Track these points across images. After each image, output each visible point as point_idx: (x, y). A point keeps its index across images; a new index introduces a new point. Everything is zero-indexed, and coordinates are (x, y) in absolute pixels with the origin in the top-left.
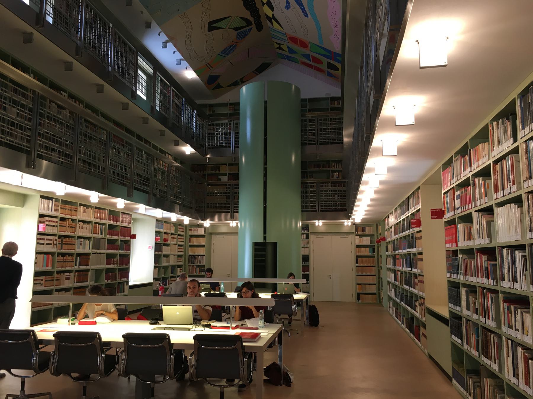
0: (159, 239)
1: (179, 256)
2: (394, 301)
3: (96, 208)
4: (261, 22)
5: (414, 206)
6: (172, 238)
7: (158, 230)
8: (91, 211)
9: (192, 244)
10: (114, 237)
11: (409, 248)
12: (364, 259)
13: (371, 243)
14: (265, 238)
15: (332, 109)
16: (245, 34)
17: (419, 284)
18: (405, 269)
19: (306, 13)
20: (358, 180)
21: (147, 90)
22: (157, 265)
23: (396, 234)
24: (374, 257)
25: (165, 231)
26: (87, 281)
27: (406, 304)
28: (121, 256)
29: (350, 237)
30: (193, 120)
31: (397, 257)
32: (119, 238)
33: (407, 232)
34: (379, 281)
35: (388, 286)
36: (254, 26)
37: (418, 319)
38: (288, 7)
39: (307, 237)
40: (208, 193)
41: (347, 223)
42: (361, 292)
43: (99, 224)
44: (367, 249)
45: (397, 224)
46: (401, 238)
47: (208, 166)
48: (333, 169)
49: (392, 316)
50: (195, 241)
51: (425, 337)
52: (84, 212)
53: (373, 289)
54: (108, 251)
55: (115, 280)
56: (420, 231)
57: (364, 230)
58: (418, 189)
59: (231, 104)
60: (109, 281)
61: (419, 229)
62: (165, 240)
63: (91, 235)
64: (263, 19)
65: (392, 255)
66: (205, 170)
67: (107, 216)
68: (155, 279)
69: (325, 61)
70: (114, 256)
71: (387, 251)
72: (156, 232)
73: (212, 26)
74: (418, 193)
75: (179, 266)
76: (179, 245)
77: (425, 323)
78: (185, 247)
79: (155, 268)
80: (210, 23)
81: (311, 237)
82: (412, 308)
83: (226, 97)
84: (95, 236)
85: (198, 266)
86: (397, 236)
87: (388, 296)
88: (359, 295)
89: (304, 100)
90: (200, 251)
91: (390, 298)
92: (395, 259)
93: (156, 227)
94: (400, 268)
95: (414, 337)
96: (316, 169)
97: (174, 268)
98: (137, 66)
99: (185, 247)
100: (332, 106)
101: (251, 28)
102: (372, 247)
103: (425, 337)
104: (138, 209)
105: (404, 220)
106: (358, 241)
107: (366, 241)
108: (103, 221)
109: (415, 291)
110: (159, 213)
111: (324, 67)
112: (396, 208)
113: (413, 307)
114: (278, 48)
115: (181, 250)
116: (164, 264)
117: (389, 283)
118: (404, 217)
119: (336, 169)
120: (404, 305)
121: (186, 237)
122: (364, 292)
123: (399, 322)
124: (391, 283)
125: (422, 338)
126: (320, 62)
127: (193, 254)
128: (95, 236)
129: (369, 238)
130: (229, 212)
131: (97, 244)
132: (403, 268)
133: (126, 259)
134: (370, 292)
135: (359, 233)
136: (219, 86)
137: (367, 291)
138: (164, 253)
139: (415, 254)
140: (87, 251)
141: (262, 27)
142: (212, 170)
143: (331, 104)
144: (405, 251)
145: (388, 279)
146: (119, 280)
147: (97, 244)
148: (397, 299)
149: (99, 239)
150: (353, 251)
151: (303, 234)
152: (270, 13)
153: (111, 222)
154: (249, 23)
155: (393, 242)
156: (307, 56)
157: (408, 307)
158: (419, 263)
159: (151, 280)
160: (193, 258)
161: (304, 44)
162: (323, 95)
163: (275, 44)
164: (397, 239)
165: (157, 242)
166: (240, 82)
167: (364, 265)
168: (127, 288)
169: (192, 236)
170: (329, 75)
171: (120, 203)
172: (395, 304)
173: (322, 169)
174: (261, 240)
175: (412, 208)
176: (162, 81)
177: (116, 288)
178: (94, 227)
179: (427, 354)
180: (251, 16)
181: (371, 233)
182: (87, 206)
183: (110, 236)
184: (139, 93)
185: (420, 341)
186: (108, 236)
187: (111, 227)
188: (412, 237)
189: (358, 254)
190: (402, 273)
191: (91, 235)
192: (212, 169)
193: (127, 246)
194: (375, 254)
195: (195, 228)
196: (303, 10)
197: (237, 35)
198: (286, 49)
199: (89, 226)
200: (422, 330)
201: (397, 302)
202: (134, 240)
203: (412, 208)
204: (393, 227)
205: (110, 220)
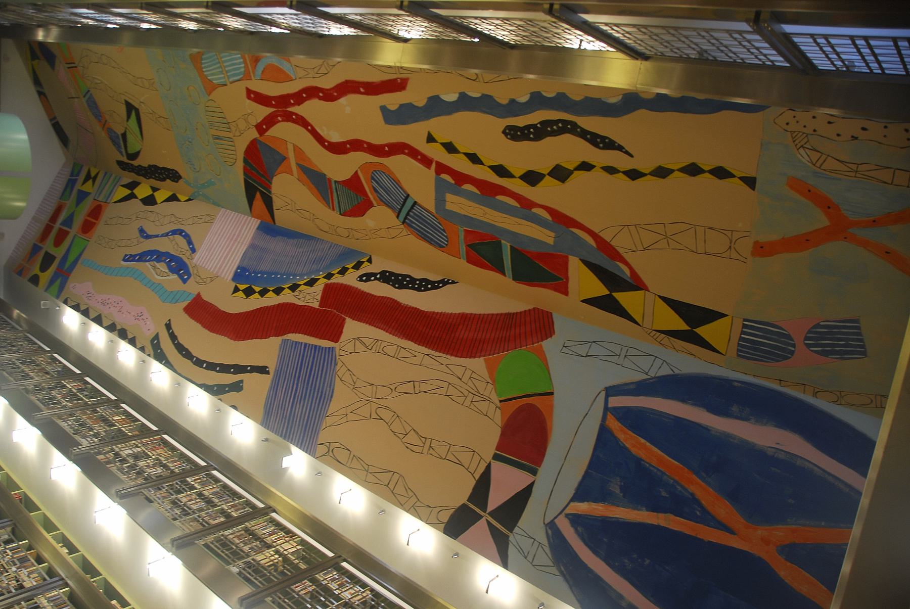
36: (125, 159)
156: (69, 221)
161: (87, 227)
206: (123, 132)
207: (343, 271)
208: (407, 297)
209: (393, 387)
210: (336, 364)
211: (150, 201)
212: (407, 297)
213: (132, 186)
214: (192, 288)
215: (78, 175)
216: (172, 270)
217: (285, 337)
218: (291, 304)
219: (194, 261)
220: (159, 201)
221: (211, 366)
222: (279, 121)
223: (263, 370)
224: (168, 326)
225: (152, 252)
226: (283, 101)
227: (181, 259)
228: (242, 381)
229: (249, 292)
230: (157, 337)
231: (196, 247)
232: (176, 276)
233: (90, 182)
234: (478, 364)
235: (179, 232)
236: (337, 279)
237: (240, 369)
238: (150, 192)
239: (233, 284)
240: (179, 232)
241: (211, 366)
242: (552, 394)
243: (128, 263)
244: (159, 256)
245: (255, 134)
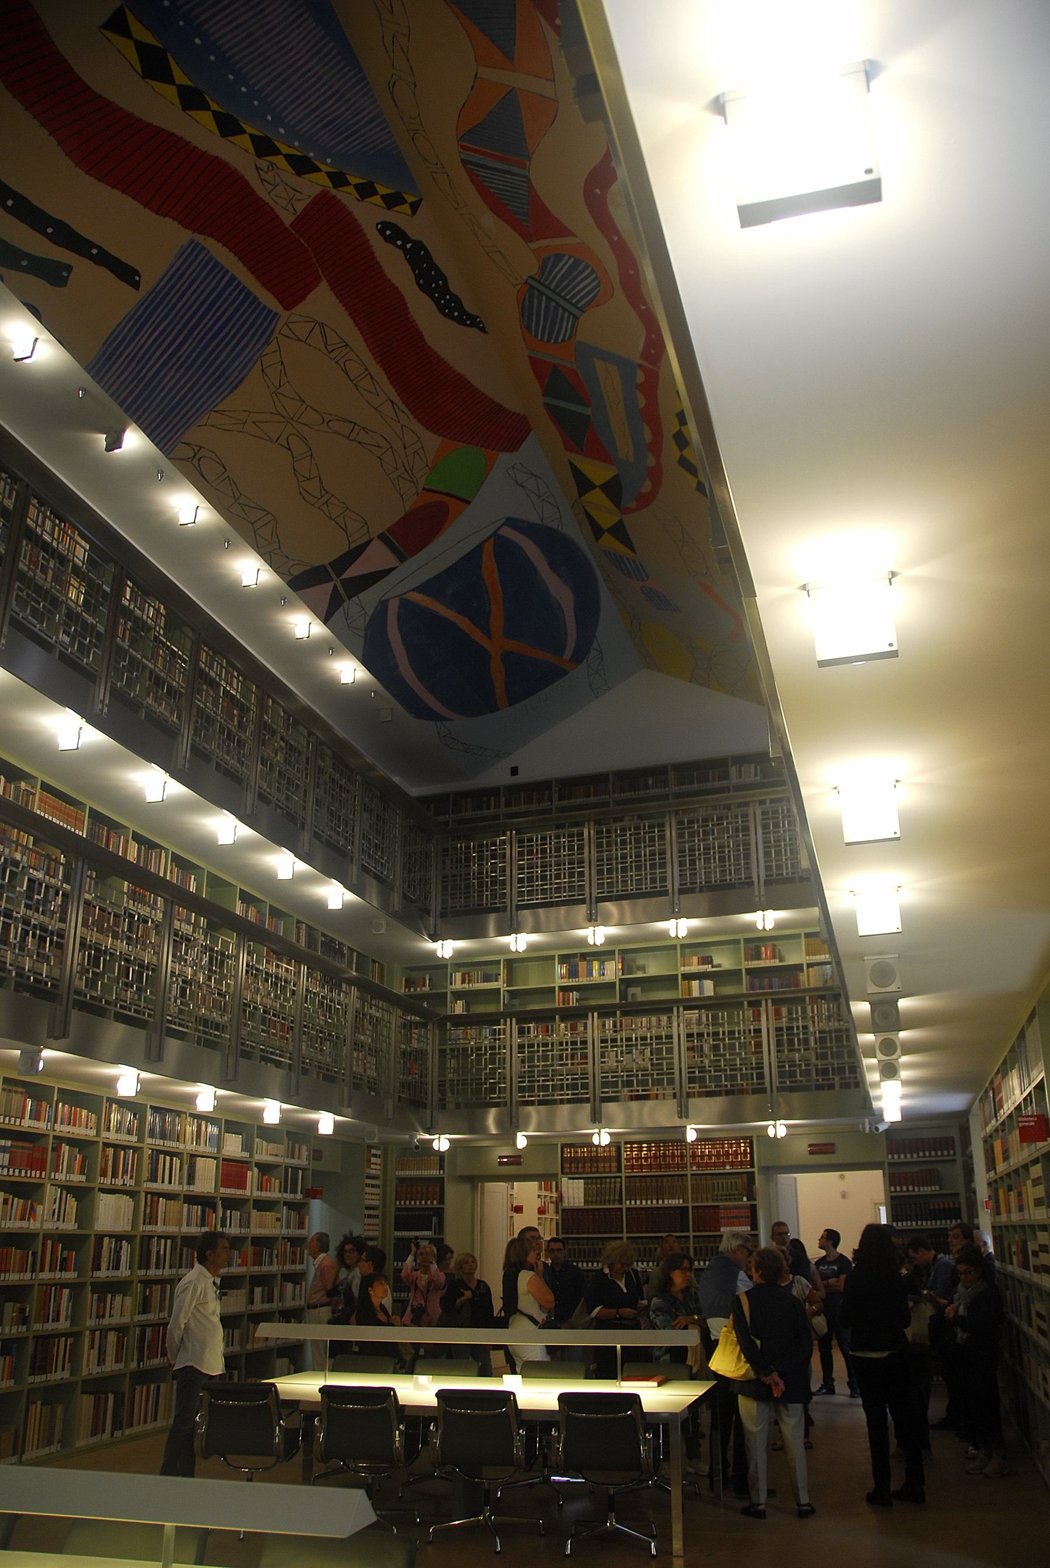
207: (366, 191)
208: (421, 309)
209: (327, 418)
210: (267, 343)
212: (421, 309)
217: (200, 238)
218: (242, 177)
223: (128, 274)
228: (69, 268)
234: (432, 441)
236: (347, 196)
242: (469, 502)
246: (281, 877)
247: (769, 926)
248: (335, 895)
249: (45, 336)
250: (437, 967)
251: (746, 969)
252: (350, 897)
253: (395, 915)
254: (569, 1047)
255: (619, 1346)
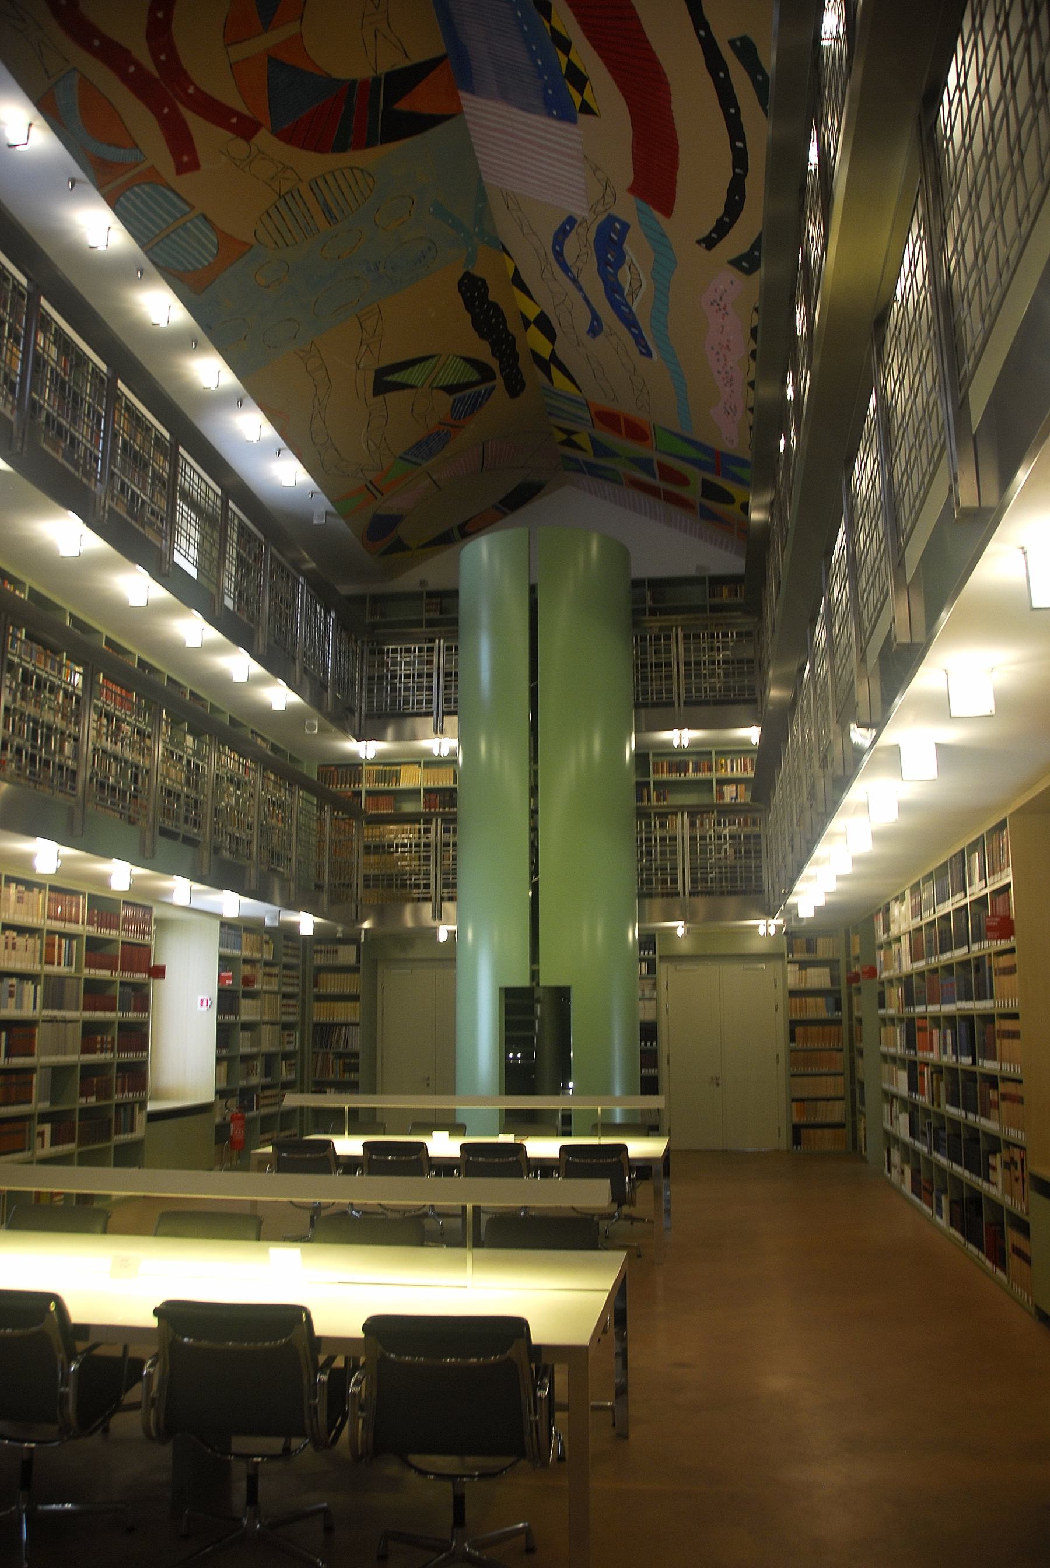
0: (228, 978)
1: (286, 1026)
2: (905, 1148)
3: (53, 889)
4: (519, 372)
5: (983, 877)
6: (265, 974)
7: (228, 951)
8: (40, 898)
9: (323, 991)
10: (104, 974)
11: (968, 998)
12: (813, 1030)
13: (832, 983)
14: (534, 975)
15: (715, 609)
16: (475, 404)
17: (1003, 1105)
18: (948, 1059)
19: (646, 347)
20: (829, 808)
21: (201, 551)
22: (225, 1052)
23: (915, 957)
24: (838, 1022)
25: (246, 954)
26: (29, 1102)
27: (954, 1158)
28: (125, 1027)
29: (776, 966)
30: (326, 637)
31: (918, 1023)
32: (118, 976)
33: (959, 954)
34: (853, 1091)
35: (886, 1107)
36: (499, 381)
37: (997, 1207)
38: (595, 329)
39: (652, 969)
40: (367, 847)
41: (766, 926)
42: (804, 1121)
43: (62, 935)
44: (820, 1001)
45: (919, 929)
46: (934, 971)
47: (365, 768)
48: (722, 774)
49: (899, 1192)
50: (332, 984)
51: (1027, 1259)
52: (20, 900)
53: (836, 1112)
54: (87, 1015)
55: (108, 1096)
56: (1011, 951)
57: (810, 947)
58: (1002, 825)
59: (431, 594)
60: (93, 1099)
61: (1003, 944)
62: (248, 981)
63: (38, 967)
64: (525, 364)
65: (901, 1020)
66: (360, 782)
67: (84, 912)
68: (220, 1093)
69: (696, 476)
70: (102, 1027)
71: (882, 1005)
72: (222, 958)
73: (384, 382)
74: (1000, 839)
75: (286, 1056)
76: (286, 996)
77: (1026, 1218)
78: (303, 1001)
79: (219, 1060)
80: (381, 373)
81: (662, 968)
82: (974, 1170)
83: (428, 573)
84: (48, 969)
85: (340, 1056)
86: (921, 964)
87: (887, 1134)
88: (797, 1130)
89: (637, 584)
90: (345, 1012)
91: (891, 1140)
92: (914, 1032)
93: (221, 945)
94: (932, 1056)
95: (983, 1257)
96: (674, 776)
97: (270, 1060)
98: (171, 488)
99: (303, 1001)
100: (717, 600)
101: (493, 388)
102: (832, 996)
103: (1027, 1259)
104: (169, 892)
105: (946, 917)
106: (793, 977)
107: (818, 978)
108: (71, 928)
109: (989, 1125)
110: (231, 904)
111: (693, 492)
112: (918, 884)
113: (984, 1171)
114: (563, 443)
115: (291, 1010)
116: (246, 1049)
117: (890, 1097)
118: (948, 907)
119: (729, 774)
120: (944, 1161)
121: (304, 971)
122: (812, 1120)
123: (926, 1207)
124: (895, 1096)
125: (1013, 1261)
126: (683, 481)
127: (325, 1019)
128: (48, 969)
129: (827, 971)
130: (427, 900)
131: (55, 992)
132: (939, 1052)
133: (137, 1036)
134: (829, 1120)
135: (798, 956)
136: (399, 546)
137: (820, 1120)
138: (244, 1017)
139: (988, 1018)
140: (27, 1012)
141: (523, 385)
142: (378, 781)
143: (712, 595)
144: (948, 1008)
145: (886, 1086)
146: (118, 1097)
147: (55, 992)
148: (918, 1144)
149: (61, 979)
150: (781, 1009)
151: (641, 960)
152: (544, 348)
153: (93, 931)
154: (485, 373)
155: (907, 982)
156: (644, 464)
157: (958, 1169)
158: (1004, 1045)
159: (207, 1095)
160: (324, 1032)
161: (636, 432)
162: (691, 571)
163: (555, 430)
164: (921, 974)
165: (226, 987)
166: (456, 533)
167: (809, 1046)
168: (140, 1119)
169: (320, 969)
170: (707, 515)
171: (120, 875)
172: (910, 1155)
173: (691, 775)
174: (525, 982)
175: (978, 884)
176: (242, 526)
177: (110, 1121)
178: (48, 945)
179: (1033, 1310)
180: (494, 354)
181: (829, 955)
182: (30, 885)
183: (93, 971)
184: (178, 558)
185: (1004, 1269)
186: (86, 971)
187: (94, 944)
188: (977, 969)
189: (795, 1016)
190: (938, 1070)
191: (38, 967)
192: (382, 777)
193: (140, 998)
194: (843, 1015)
195: (331, 948)
196: (639, 339)
197: (454, 407)
198: (587, 444)
199: (34, 943)
200: (1012, 1237)
201: (917, 1153)
202: (161, 981)
203: (978, 884)
204: (905, 940)
205: (90, 923)
206: (443, 394)
211: (543, 323)
213: (542, 364)
214: (628, 208)
215: (577, 461)
216: (621, 258)
219: (586, 214)
220: (537, 312)
221: (735, 129)
222: (197, 88)
224: (709, 242)
225: (615, 305)
226: (140, 85)
227: (596, 240)
229: (579, 79)
230: (736, 263)
231: (564, 218)
232: (626, 246)
233: (575, 438)
235: (559, 255)
237: (714, 62)
238: (533, 328)
239: (582, 118)
240: (559, 255)
241: (735, 129)
243: (650, 344)
244: (613, 290)
245: (264, 138)
246: (236, 679)
247: (686, 743)
248: (279, 696)
249: (40, 122)
250: (352, 767)
251: (366, 792)
252: (295, 699)
253: (327, 715)
254: (414, 849)
255: (347, 1108)
